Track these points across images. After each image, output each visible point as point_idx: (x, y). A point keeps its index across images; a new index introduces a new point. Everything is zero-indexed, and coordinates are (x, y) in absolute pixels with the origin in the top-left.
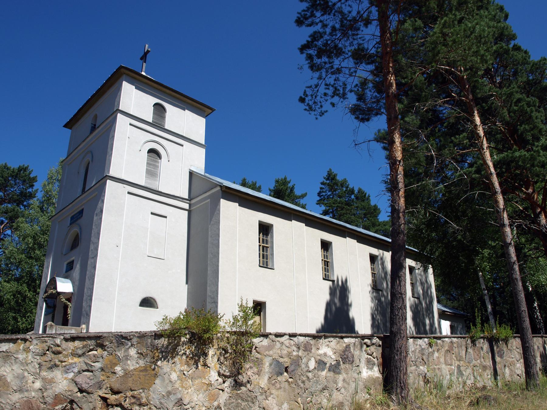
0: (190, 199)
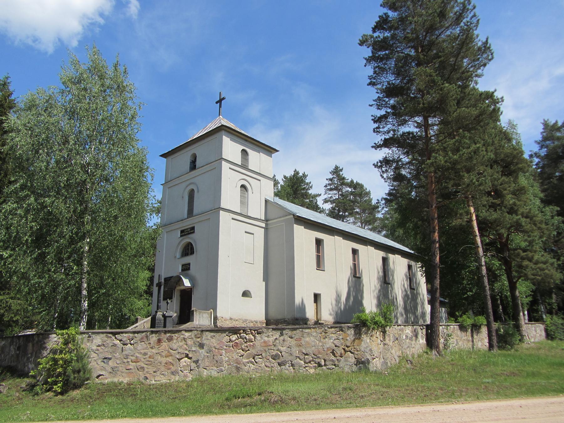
0: (266, 220)
